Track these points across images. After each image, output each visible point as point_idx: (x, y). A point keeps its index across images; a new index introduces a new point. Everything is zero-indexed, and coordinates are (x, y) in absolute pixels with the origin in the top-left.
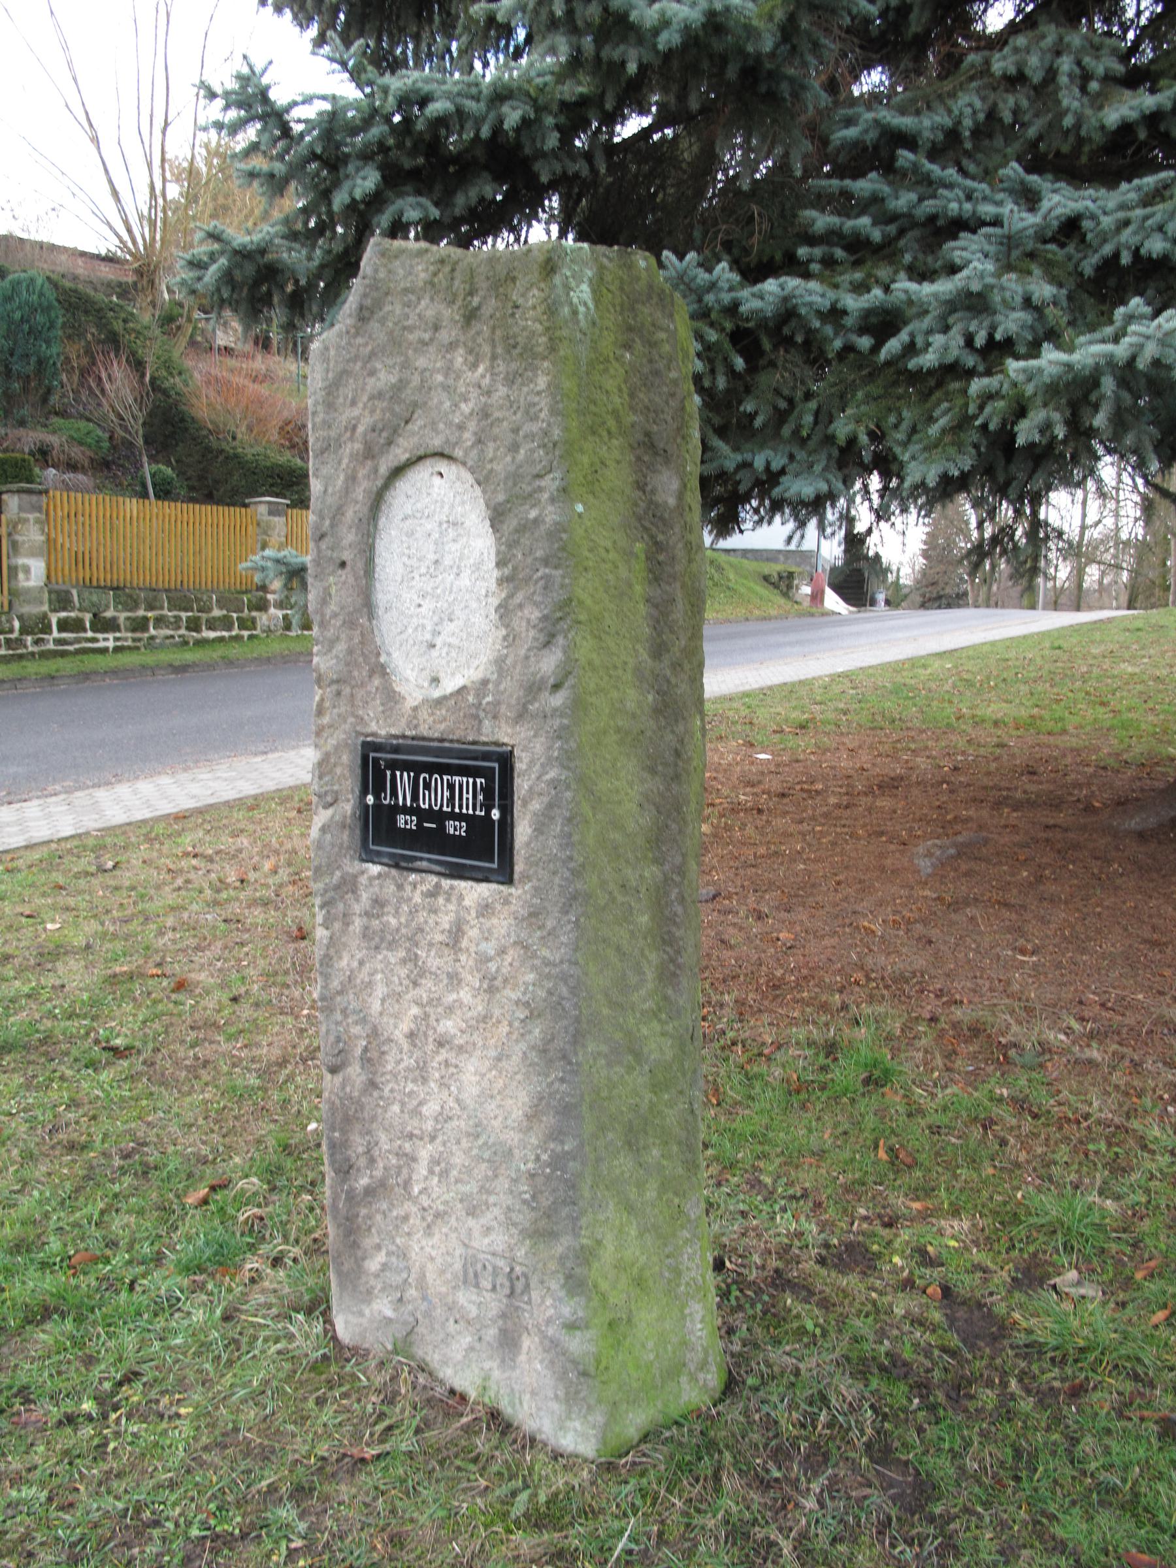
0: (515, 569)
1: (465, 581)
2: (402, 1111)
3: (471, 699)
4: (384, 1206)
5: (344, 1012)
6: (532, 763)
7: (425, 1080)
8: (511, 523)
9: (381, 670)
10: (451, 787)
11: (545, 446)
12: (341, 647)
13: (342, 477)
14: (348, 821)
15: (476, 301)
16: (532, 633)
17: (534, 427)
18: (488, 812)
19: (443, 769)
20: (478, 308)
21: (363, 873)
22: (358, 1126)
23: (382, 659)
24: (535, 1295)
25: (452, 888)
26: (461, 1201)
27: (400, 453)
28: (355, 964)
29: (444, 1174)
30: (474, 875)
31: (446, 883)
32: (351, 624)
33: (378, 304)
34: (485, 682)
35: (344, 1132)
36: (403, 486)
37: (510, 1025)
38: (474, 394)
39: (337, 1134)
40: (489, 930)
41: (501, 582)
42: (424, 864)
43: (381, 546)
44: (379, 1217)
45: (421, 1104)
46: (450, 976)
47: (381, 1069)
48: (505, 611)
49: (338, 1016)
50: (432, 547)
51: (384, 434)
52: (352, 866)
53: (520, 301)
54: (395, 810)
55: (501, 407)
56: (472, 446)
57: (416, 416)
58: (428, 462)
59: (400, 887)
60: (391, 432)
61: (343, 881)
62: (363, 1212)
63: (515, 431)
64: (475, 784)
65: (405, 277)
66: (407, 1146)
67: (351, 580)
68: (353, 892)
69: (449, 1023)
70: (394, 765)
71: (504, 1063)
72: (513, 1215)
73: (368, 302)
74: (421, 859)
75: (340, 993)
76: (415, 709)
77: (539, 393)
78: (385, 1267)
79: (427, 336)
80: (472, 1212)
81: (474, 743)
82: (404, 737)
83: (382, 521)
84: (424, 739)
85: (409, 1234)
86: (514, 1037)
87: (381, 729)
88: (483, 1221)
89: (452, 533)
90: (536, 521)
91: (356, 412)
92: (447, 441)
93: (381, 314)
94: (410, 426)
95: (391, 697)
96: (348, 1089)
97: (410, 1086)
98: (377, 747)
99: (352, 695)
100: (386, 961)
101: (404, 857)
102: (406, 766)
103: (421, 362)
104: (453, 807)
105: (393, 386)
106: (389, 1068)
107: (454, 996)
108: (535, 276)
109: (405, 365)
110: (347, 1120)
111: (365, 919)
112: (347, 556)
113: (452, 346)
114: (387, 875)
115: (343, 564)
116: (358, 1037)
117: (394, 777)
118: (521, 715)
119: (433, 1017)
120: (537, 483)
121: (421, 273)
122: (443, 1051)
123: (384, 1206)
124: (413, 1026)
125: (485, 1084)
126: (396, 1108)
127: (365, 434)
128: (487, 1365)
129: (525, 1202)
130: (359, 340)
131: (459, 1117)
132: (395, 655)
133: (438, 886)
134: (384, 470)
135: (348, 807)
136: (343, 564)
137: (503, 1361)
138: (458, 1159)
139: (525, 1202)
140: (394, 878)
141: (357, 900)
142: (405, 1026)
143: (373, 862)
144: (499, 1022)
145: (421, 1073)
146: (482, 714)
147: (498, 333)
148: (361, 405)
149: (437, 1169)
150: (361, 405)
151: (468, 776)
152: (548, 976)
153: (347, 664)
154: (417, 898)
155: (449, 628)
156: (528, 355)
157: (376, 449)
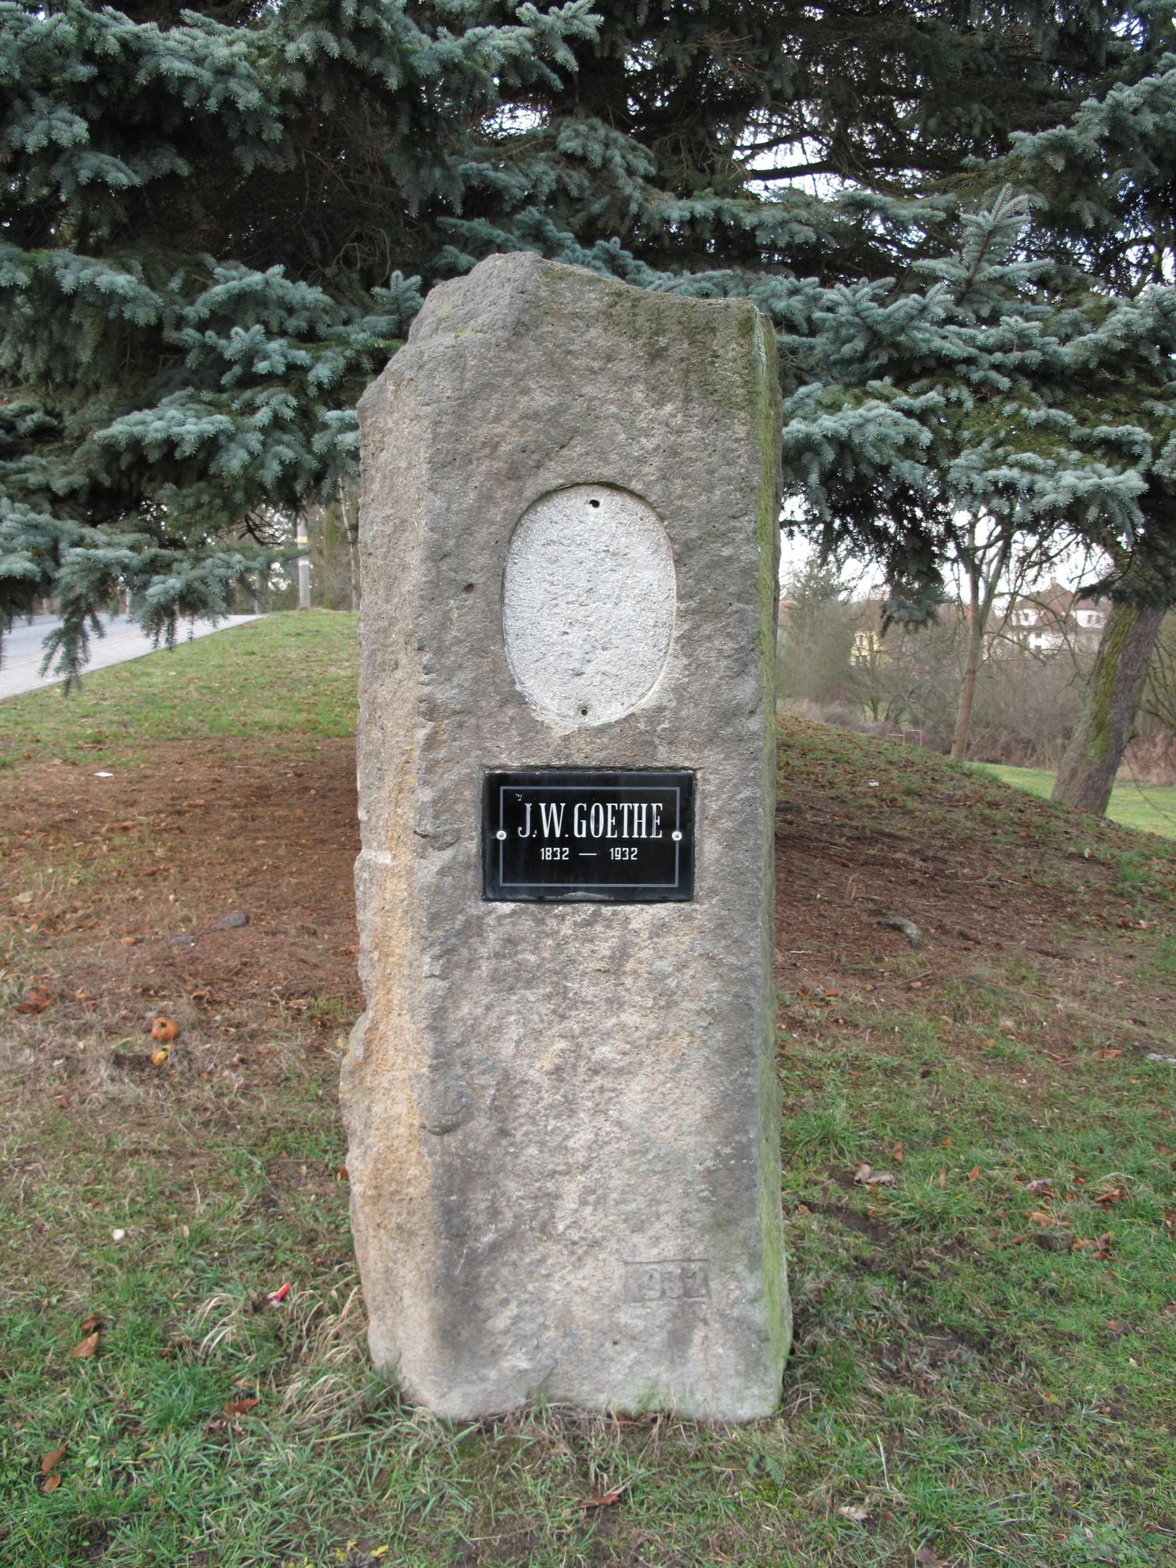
0: (702, 601)
1: (627, 609)
2: (541, 1152)
3: (642, 726)
4: (514, 1256)
5: (467, 1064)
6: (723, 784)
7: (572, 1113)
8: (699, 561)
9: (520, 700)
10: (618, 814)
11: (741, 490)
12: (464, 677)
13: (472, 495)
14: (474, 860)
15: (663, 341)
16: (724, 663)
17: (733, 471)
18: (668, 835)
19: (604, 798)
20: (665, 349)
21: (490, 913)
22: (480, 1182)
23: (518, 688)
24: (714, 1285)
25: (615, 913)
26: (625, 1221)
27: (550, 477)
28: (480, 1011)
29: (600, 1201)
30: (648, 897)
31: (607, 910)
32: (480, 651)
33: (536, 323)
34: (660, 709)
35: (462, 1192)
36: (546, 511)
37: (692, 1034)
38: (659, 430)
39: (454, 1198)
40: (665, 949)
41: (682, 615)
42: (580, 894)
43: (512, 571)
44: (505, 1271)
45: (567, 1137)
46: (609, 1001)
47: (512, 1115)
48: (687, 642)
49: (459, 1070)
50: (584, 576)
51: (535, 457)
52: (477, 907)
53: (721, 352)
54: (539, 842)
55: (694, 448)
56: (656, 481)
57: (573, 443)
58: (583, 490)
59: (541, 922)
60: (544, 455)
61: (468, 924)
62: (485, 1271)
63: (711, 472)
64: (649, 809)
65: (574, 301)
66: (550, 1186)
67: (481, 604)
68: (479, 935)
69: (604, 1049)
70: (535, 798)
71: (683, 1074)
72: (690, 1216)
73: (526, 318)
74: (575, 890)
75: (459, 1045)
76: (566, 738)
77: (737, 440)
78: (516, 1319)
79: (596, 365)
80: (639, 1228)
81: (646, 768)
82: (548, 767)
83: (517, 545)
84: (576, 768)
85: (548, 1276)
86: (695, 1045)
87: (510, 760)
88: (651, 1233)
89: (610, 564)
90: (729, 559)
91: (499, 429)
92: (622, 472)
93: (538, 332)
94: (565, 452)
95: (532, 728)
96: (471, 1145)
97: (552, 1123)
98: (503, 779)
99: (478, 727)
100: (523, 1001)
101: (550, 890)
102: (551, 798)
103: (589, 390)
104: (621, 833)
105: (553, 409)
106: (523, 1111)
107: (614, 1020)
108: (734, 331)
109: (568, 388)
110: (469, 1178)
111: (494, 961)
112: (474, 578)
113: (632, 380)
114: (523, 911)
115: (469, 587)
116: (484, 1087)
117: (536, 812)
118: (712, 739)
119: (586, 1046)
120: (732, 523)
121: (593, 300)
122: (597, 1078)
123: (514, 1256)
124: (557, 1061)
125: (656, 1098)
126: (533, 1150)
127: (512, 453)
128: (653, 1372)
129: (703, 1200)
130: (510, 355)
131: (619, 1139)
132: (529, 684)
133: (596, 915)
134: (530, 492)
135: (472, 846)
136: (469, 587)
137: (672, 1362)
138: (618, 1180)
139: (703, 1200)
140: (532, 914)
141: (483, 943)
142: (547, 1062)
143: (503, 900)
144: (676, 1034)
145: (569, 1108)
146: (657, 741)
147: (693, 376)
148: (506, 422)
149: (592, 1198)
150: (506, 422)
151: (640, 802)
152: (733, 982)
153: (473, 694)
154: (566, 930)
155: (602, 656)
156: (726, 404)
157: (523, 471)
